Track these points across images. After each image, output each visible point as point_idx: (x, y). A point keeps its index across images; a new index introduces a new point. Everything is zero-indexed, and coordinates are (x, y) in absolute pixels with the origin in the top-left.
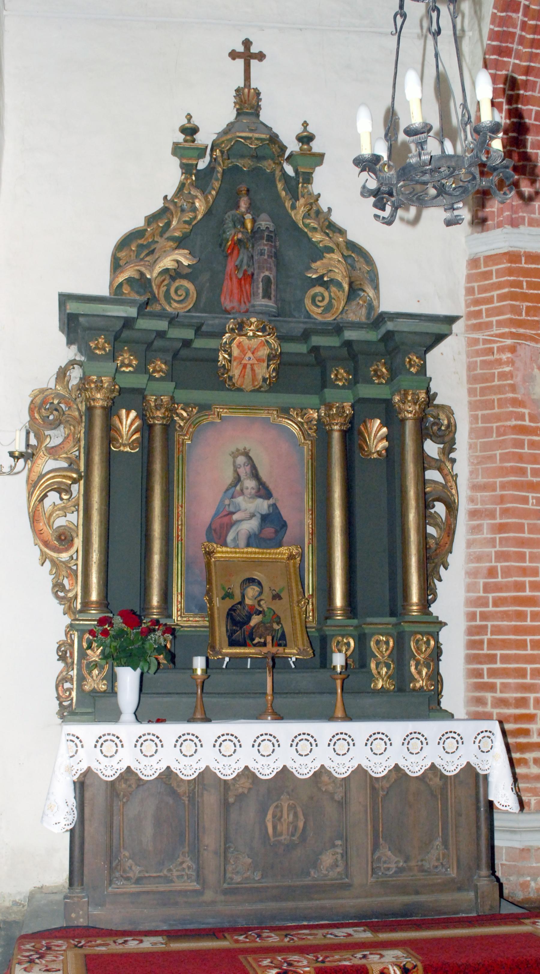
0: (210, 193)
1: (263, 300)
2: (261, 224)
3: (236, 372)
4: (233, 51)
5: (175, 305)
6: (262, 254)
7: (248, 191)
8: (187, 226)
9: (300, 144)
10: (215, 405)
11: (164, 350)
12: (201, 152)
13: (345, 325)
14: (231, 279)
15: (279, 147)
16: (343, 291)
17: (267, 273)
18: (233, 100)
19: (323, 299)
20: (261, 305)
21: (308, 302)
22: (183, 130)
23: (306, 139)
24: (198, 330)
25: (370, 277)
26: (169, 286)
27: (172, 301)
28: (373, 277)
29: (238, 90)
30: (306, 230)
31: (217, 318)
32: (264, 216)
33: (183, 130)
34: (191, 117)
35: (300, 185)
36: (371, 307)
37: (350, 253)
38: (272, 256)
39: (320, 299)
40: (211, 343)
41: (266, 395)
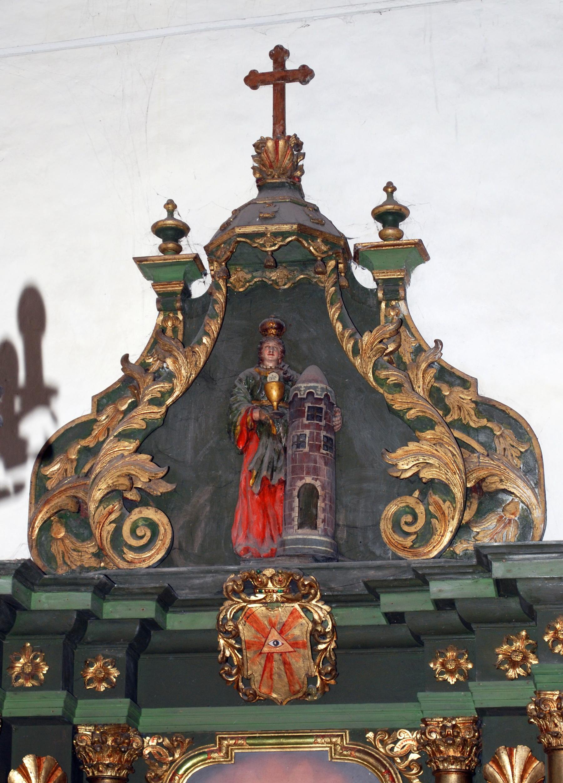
0: (200, 342)
1: (300, 531)
2: (298, 389)
3: (255, 669)
4: (253, 73)
5: (130, 555)
6: (299, 444)
7: (280, 327)
8: (155, 409)
9: (380, 226)
10: (222, 732)
11: (107, 641)
12: (195, 267)
13: (427, 571)
14: (246, 497)
15: (325, 241)
16: (453, 500)
17: (309, 480)
18: (251, 163)
19: (415, 518)
20: (296, 541)
21: (385, 526)
22: (159, 230)
23: (390, 216)
24: (167, 600)
25: (526, 464)
26: (119, 522)
27: (125, 550)
28: (532, 463)
29: (260, 146)
30: (381, 391)
31: (210, 572)
32: (312, 371)
33: (159, 230)
34: (175, 207)
35: (383, 305)
36: (526, 524)
37: (484, 422)
38: (318, 448)
39: (409, 518)
40: (203, 621)
41: (321, 708)
